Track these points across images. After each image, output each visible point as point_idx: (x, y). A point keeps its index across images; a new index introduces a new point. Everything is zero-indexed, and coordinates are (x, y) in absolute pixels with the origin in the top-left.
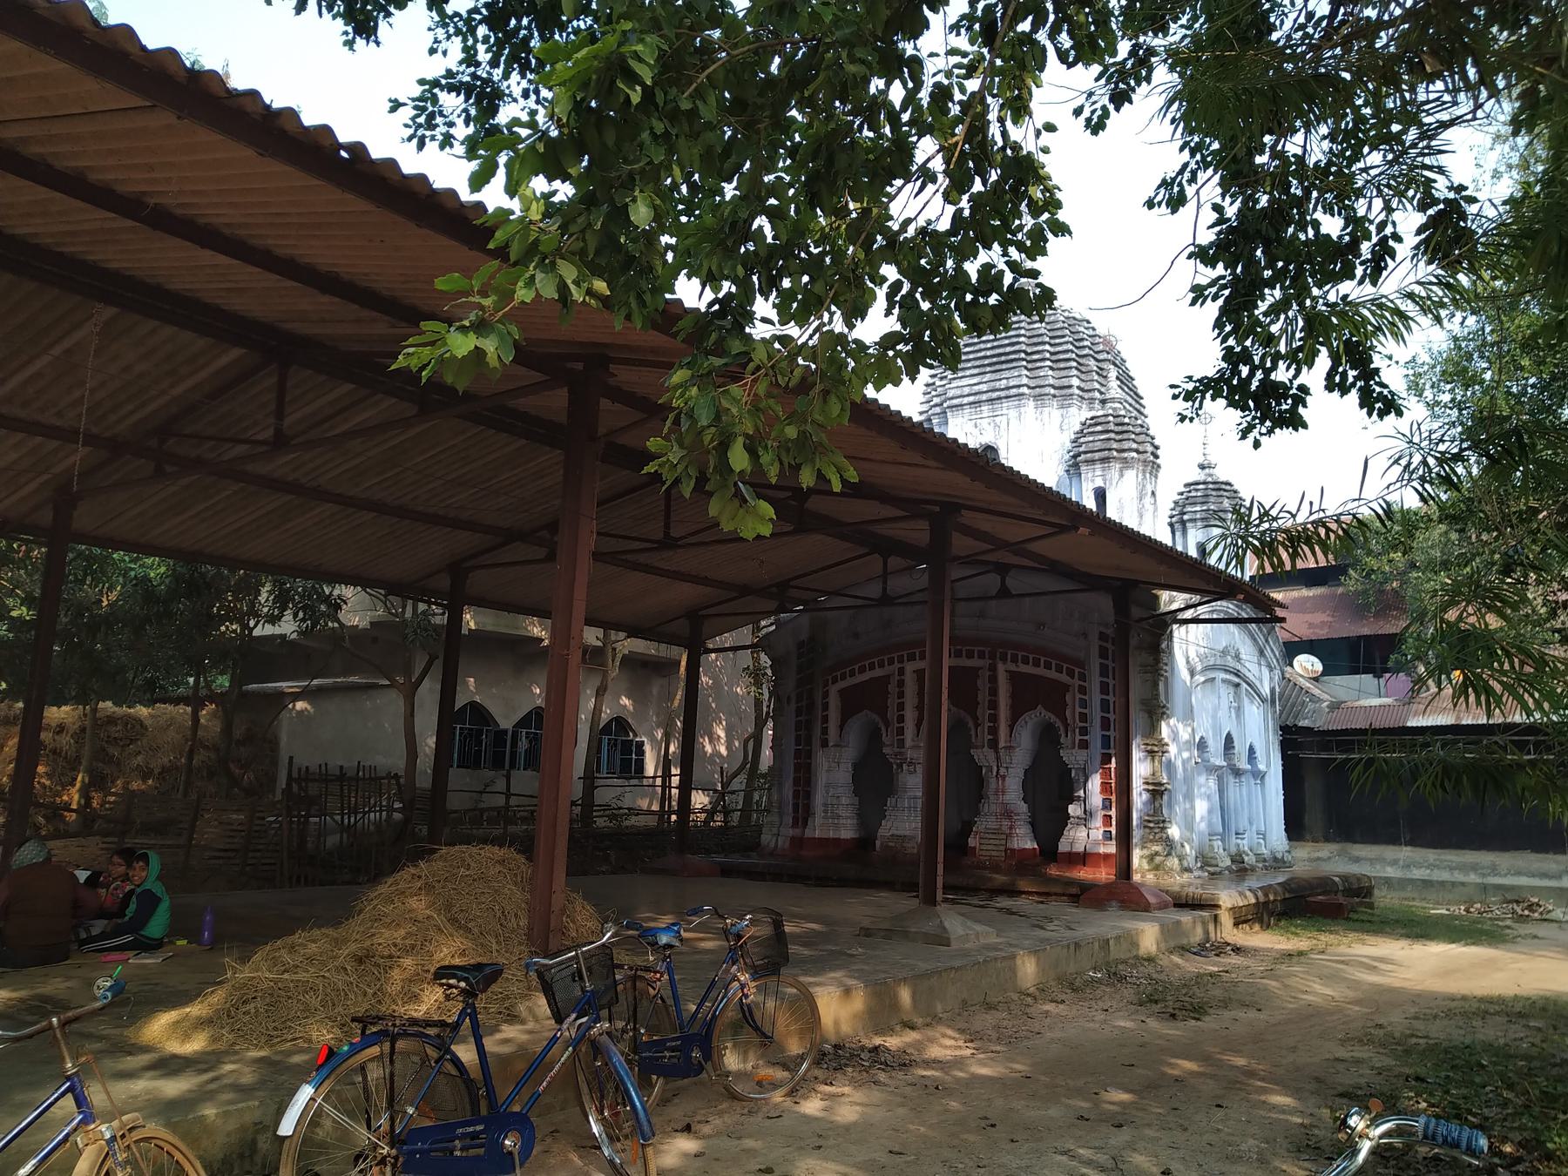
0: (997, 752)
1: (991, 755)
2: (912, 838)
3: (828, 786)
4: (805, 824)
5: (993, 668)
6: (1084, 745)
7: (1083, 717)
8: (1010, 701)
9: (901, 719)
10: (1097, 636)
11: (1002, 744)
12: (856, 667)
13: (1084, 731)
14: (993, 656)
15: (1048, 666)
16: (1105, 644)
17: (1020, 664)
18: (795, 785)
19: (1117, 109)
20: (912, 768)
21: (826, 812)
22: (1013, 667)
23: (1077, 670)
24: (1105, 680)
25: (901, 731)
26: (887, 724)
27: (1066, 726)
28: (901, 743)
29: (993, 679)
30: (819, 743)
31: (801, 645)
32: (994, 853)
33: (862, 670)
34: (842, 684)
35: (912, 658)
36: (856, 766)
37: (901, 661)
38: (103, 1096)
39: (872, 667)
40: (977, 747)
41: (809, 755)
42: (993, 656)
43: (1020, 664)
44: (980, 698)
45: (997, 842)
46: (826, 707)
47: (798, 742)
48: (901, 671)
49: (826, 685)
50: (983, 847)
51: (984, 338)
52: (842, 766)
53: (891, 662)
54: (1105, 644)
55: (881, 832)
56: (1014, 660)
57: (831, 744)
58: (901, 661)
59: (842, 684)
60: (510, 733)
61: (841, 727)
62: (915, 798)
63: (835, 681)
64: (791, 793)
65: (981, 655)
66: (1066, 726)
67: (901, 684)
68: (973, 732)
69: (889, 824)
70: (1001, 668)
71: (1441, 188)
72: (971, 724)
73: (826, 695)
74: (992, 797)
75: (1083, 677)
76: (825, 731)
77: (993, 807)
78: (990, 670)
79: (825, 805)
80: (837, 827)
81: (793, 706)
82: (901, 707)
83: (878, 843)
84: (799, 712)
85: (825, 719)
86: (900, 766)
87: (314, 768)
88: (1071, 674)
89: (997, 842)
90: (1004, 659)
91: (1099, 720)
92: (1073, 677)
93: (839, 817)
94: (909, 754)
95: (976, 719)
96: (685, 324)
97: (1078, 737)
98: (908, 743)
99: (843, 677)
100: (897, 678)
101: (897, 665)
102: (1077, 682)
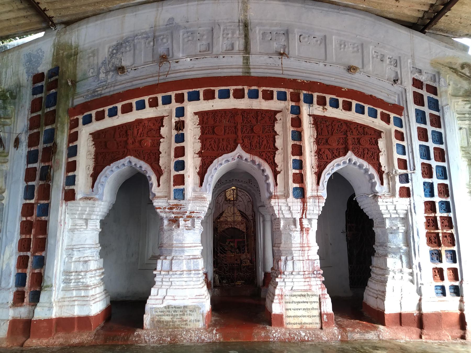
0: (304, 202)
1: (296, 205)
2: (194, 309)
3: (71, 249)
4: (35, 299)
5: (296, 111)
6: (406, 193)
7: (403, 164)
8: (315, 148)
9: (180, 166)
10: (411, 82)
11: (309, 193)
13: (405, 178)
14: (296, 98)
15: (360, 110)
20: (189, 223)
21: (67, 281)
22: (318, 110)
23: (392, 115)
24: (423, 126)
25: (180, 180)
26: (159, 173)
27: (381, 173)
28: (181, 194)
29: (297, 123)
30: (61, 195)
31: (38, 78)
33: (127, 109)
34: (97, 126)
35: (194, 97)
37: (180, 99)
38: (161, 200)
39: (141, 106)
41: (45, 210)
42: (296, 98)
43: (328, 106)
44: (279, 143)
45: (308, 306)
46: (73, 151)
47: (29, 192)
48: (181, 112)
49: (75, 124)
50: (290, 313)
51: (64, 252)
52: (91, 223)
53: (167, 101)
55: (151, 303)
56: (322, 102)
57: (79, 196)
58: (180, 99)
59: (97, 126)
61: (94, 176)
62: (195, 258)
63: (87, 121)
65: (282, 97)
66: (381, 173)
67: (180, 126)
68: (271, 180)
69: (162, 292)
70: (305, 109)
71: (317, 34)
72: (269, 172)
73: (74, 137)
74: (296, 255)
75: (399, 123)
76: (71, 181)
78: (292, 112)
79: (67, 273)
80: (85, 301)
81: (24, 149)
82: (180, 152)
83: (147, 319)
84: (32, 157)
85: (72, 167)
86: (175, 221)
88: (386, 119)
89: (308, 306)
90: (309, 100)
92: (388, 122)
94: (190, 207)
95: (273, 166)
97: (398, 185)
99: (100, 117)
100: (174, 120)
101: (174, 105)
102: (393, 127)
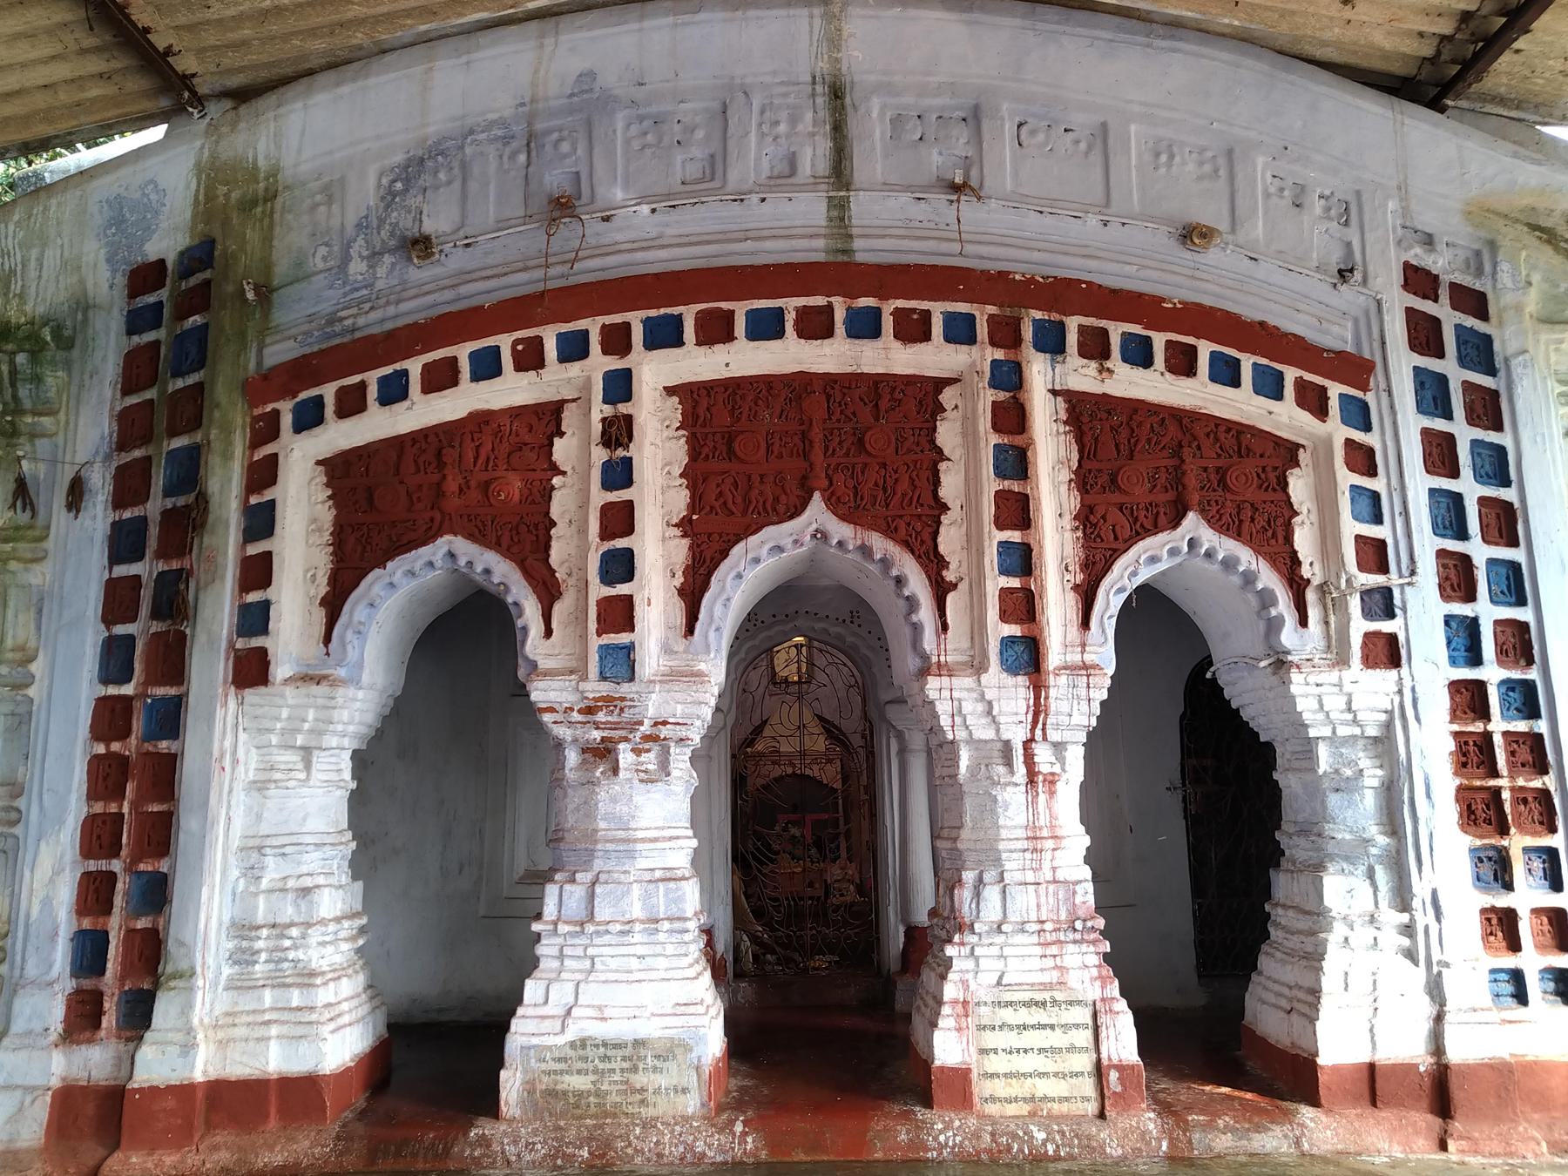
0: (1038, 686)
2: (670, 1051)
3: (255, 849)
4: (138, 1016)
5: (1010, 377)
6: (1387, 652)
7: (1374, 555)
8: (1073, 502)
9: (620, 566)
10: (1397, 277)
11: (1054, 656)
13: (1382, 603)
15: (1227, 373)
18: (88, 850)
19: (1456, 735)
20: (650, 760)
21: (242, 958)
22: (1082, 376)
23: (1335, 390)
24: (1440, 424)
25: (619, 615)
27: (1297, 586)
28: (622, 663)
29: (1013, 417)
31: (145, 277)
32: (1044, 1087)
33: (441, 378)
34: (340, 435)
35: (665, 336)
37: (617, 341)
39: (487, 367)
41: (170, 719)
42: (1004, 332)
43: (1115, 363)
44: (951, 485)
45: (1056, 1039)
46: (261, 521)
48: (620, 386)
49: (267, 430)
50: (996, 1064)
53: (574, 349)
56: (1096, 347)
57: (281, 670)
58: (617, 341)
59: (340, 435)
62: (670, 877)
63: (309, 418)
64: (65, 894)
65: (960, 331)
66: (1297, 586)
67: (618, 432)
69: (561, 994)
70: (1039, 373)
72: (918, 584)
73: (264, 474)
75: (1359, 415)
76: (255, 619)
78: (995, 384)
79: (243, 929)
80: (302, 1023)
81: (98, 517)
82: (620, 520)
83: (511, 1084)
84: (124, 542)
85: (258, 572)
86: (603, 753)
88: (1314, 401)
89: (1056, 1039)
90: (1052, 343)
91: (1424, 499)
92: (1321, 412)
94: (654, 705)
95: (933, 563)
96: (1090, 499)
97: (1360, 626)
99: (351, 404)
101: (599, 363)
102: (1338, 431)
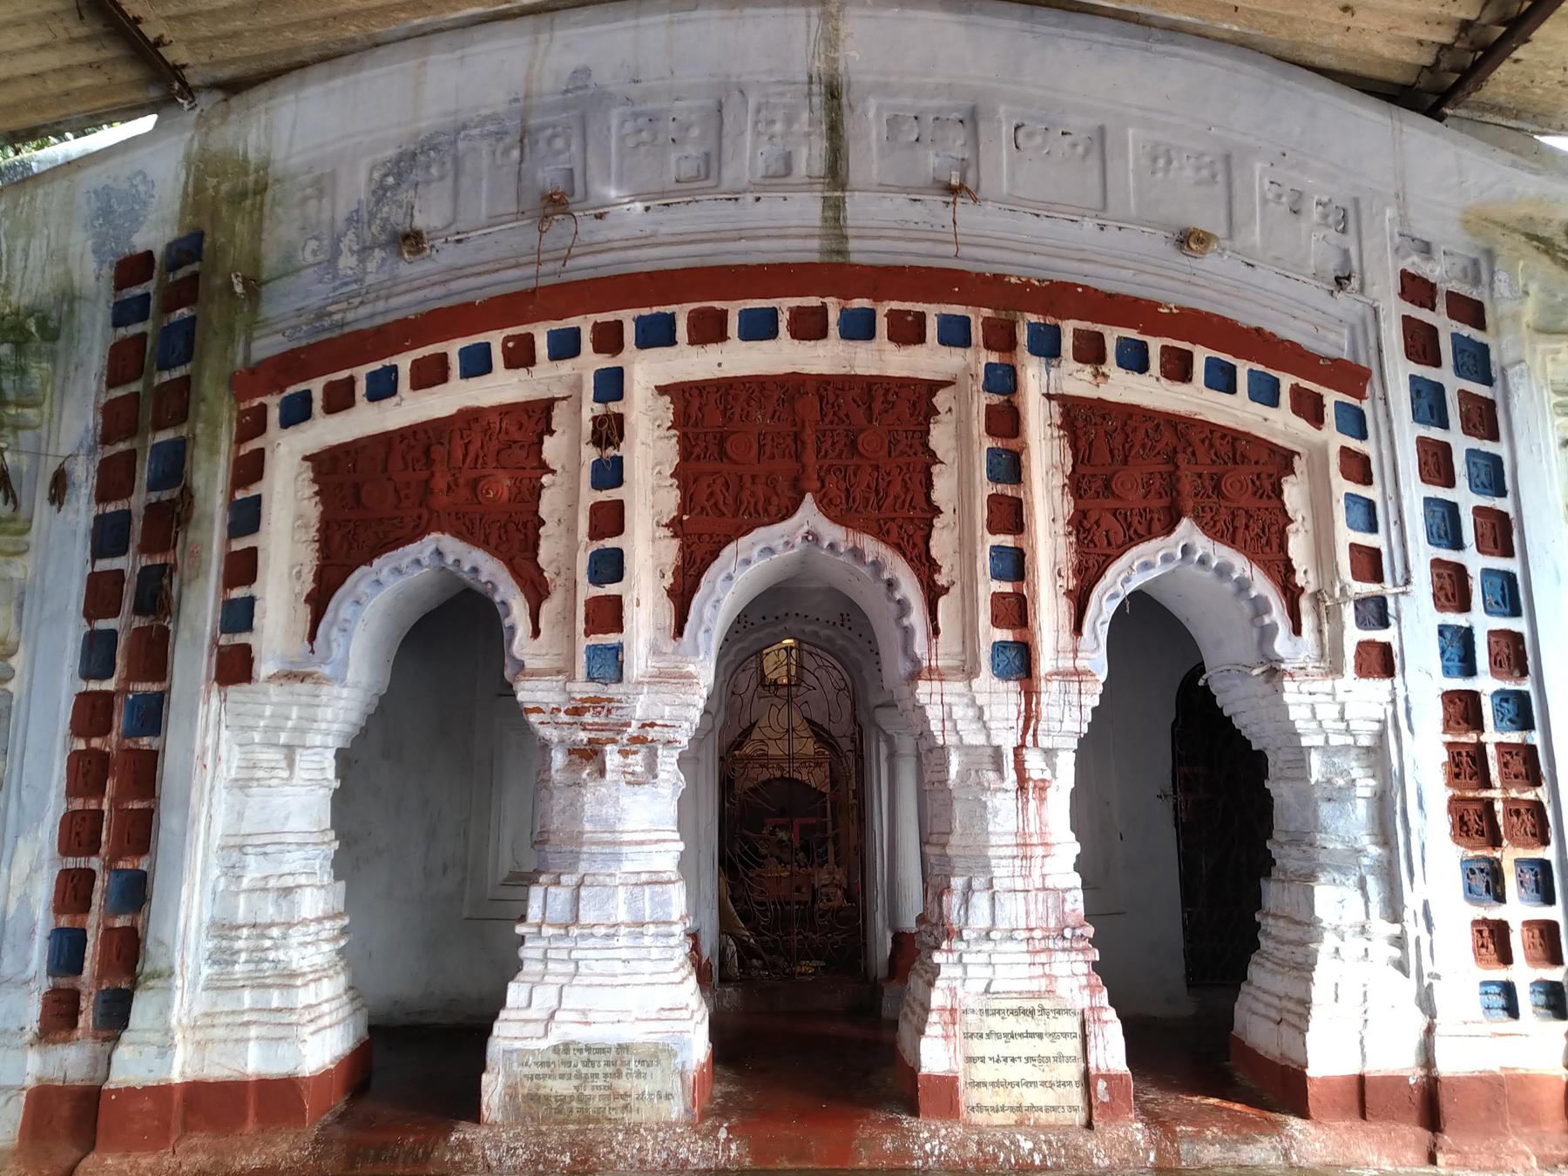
2: (654, 1056)
3: (236, 848)
4: (115, 1016)
5: (1004, 381)
7: (1369, 564)
8: (1067, 507)
9: (610, 566)
10: (1394, 284)
11: (1046, 662)
12: (317, 387)
13: (1376, 612)
15: (1222, 379)
16: (1423, 315)
17: (1111, 366)
20: (637, 762)
21: (223, 958)
22: (1077, 380)
23: (1331, 398)
24: (1436, 433)
25: (608, 615)
27: (1292, 595)
28: (610, 664)
29: (1006, 421)
33: (431, 374)
35: (657, 334)
36: (345, 760)
37: (608, 340)
39: (477, 364)
40: (935, 674)
41: (152, 715)
42: (1001, 337)
43: (1111, 366)
45: (1045, 1048)
46: (246, 517)
48: (611, 385)
49: (254, 425)
50: (982, 1072)
52: (304, 759)
54: (1423, 315)
55: (506, 1036)
56: (1090, 351)
57: (265, 667)
58: (608, 340)
60: (176, 1123)
61: (318, 602)
63: (297, 413)
65: (955, 334)
66: (1292, 595)
67: (609, 431)
69: (545, 998)
70: (1034, 377)
72: (909, 588)
73: (250, 469)
75: (1355, 423)
76: (239, 615)
77: (1013, 911)
78: (989, 387)
79: (223, 929)
80: (282, 1024)
81: (81, 510)
82: (609, 519)
83: (493, 1088)
85: (243, 568)
86: (590, 754)
87: (1027, 765)
88: (1310, 409)
89: (1045, 1048)
90: (1048, 347)
92: (1317, 419)
93: (288, 978)
94: (642, 706)
95: (925, 567)
97: (1353, 635)
98: (639, 660)
99: (340, 399)
100: (590, 409)
101: (590, 361)
102: (1333, 439)
